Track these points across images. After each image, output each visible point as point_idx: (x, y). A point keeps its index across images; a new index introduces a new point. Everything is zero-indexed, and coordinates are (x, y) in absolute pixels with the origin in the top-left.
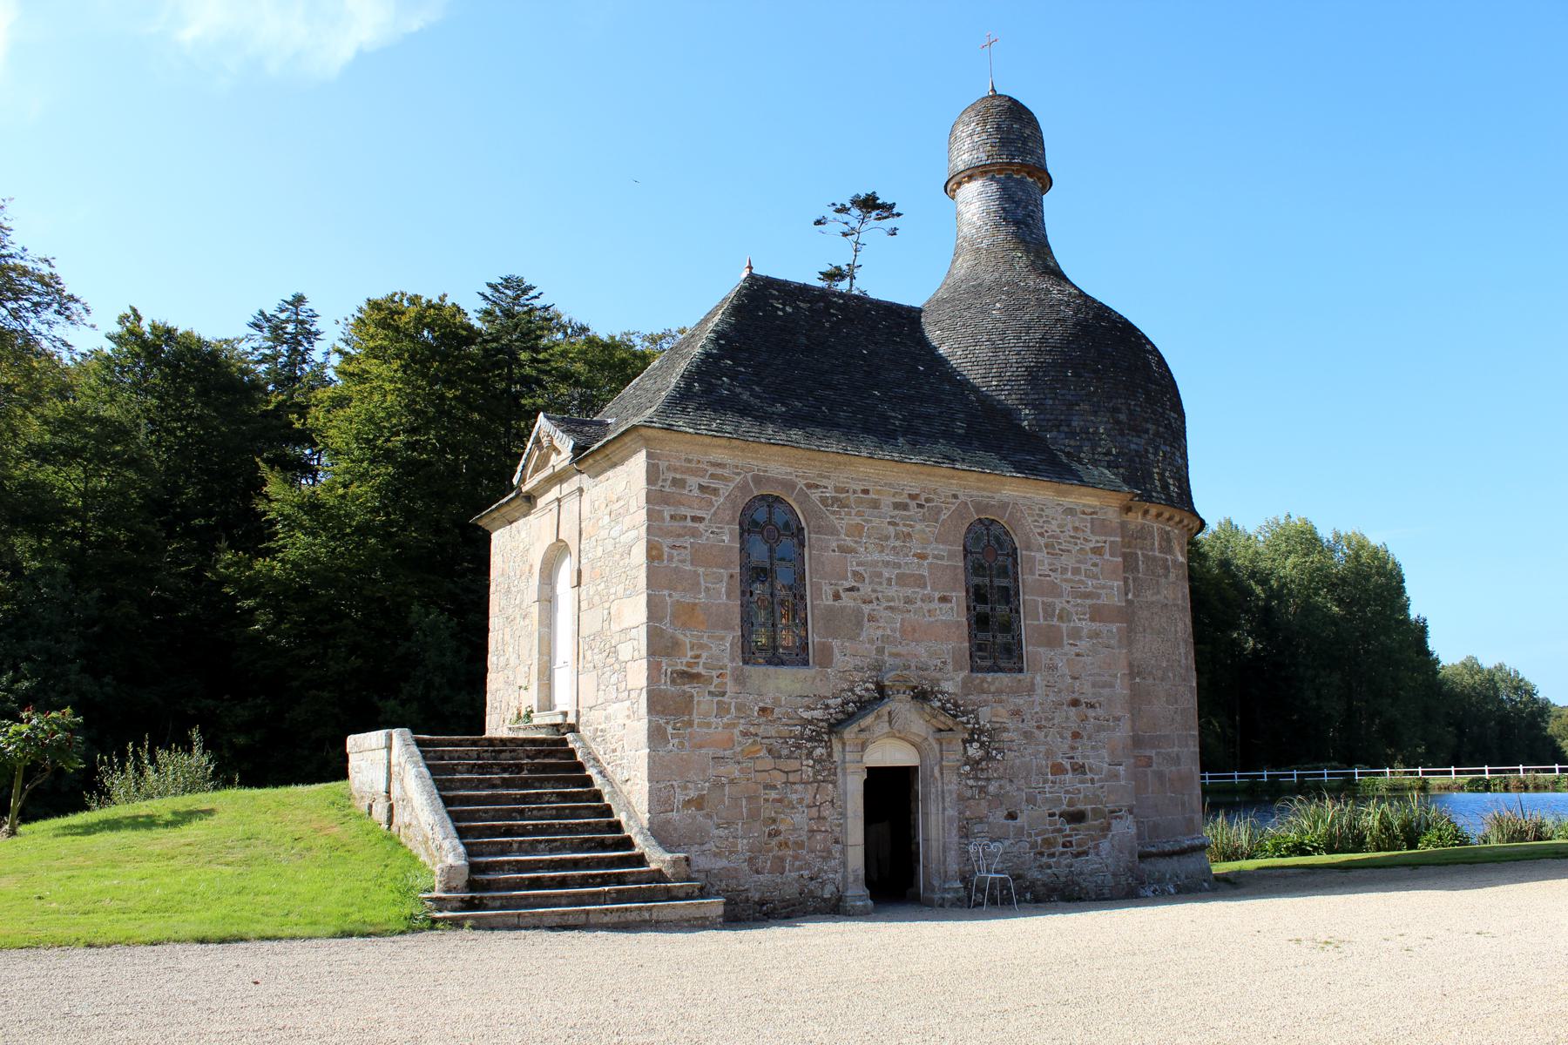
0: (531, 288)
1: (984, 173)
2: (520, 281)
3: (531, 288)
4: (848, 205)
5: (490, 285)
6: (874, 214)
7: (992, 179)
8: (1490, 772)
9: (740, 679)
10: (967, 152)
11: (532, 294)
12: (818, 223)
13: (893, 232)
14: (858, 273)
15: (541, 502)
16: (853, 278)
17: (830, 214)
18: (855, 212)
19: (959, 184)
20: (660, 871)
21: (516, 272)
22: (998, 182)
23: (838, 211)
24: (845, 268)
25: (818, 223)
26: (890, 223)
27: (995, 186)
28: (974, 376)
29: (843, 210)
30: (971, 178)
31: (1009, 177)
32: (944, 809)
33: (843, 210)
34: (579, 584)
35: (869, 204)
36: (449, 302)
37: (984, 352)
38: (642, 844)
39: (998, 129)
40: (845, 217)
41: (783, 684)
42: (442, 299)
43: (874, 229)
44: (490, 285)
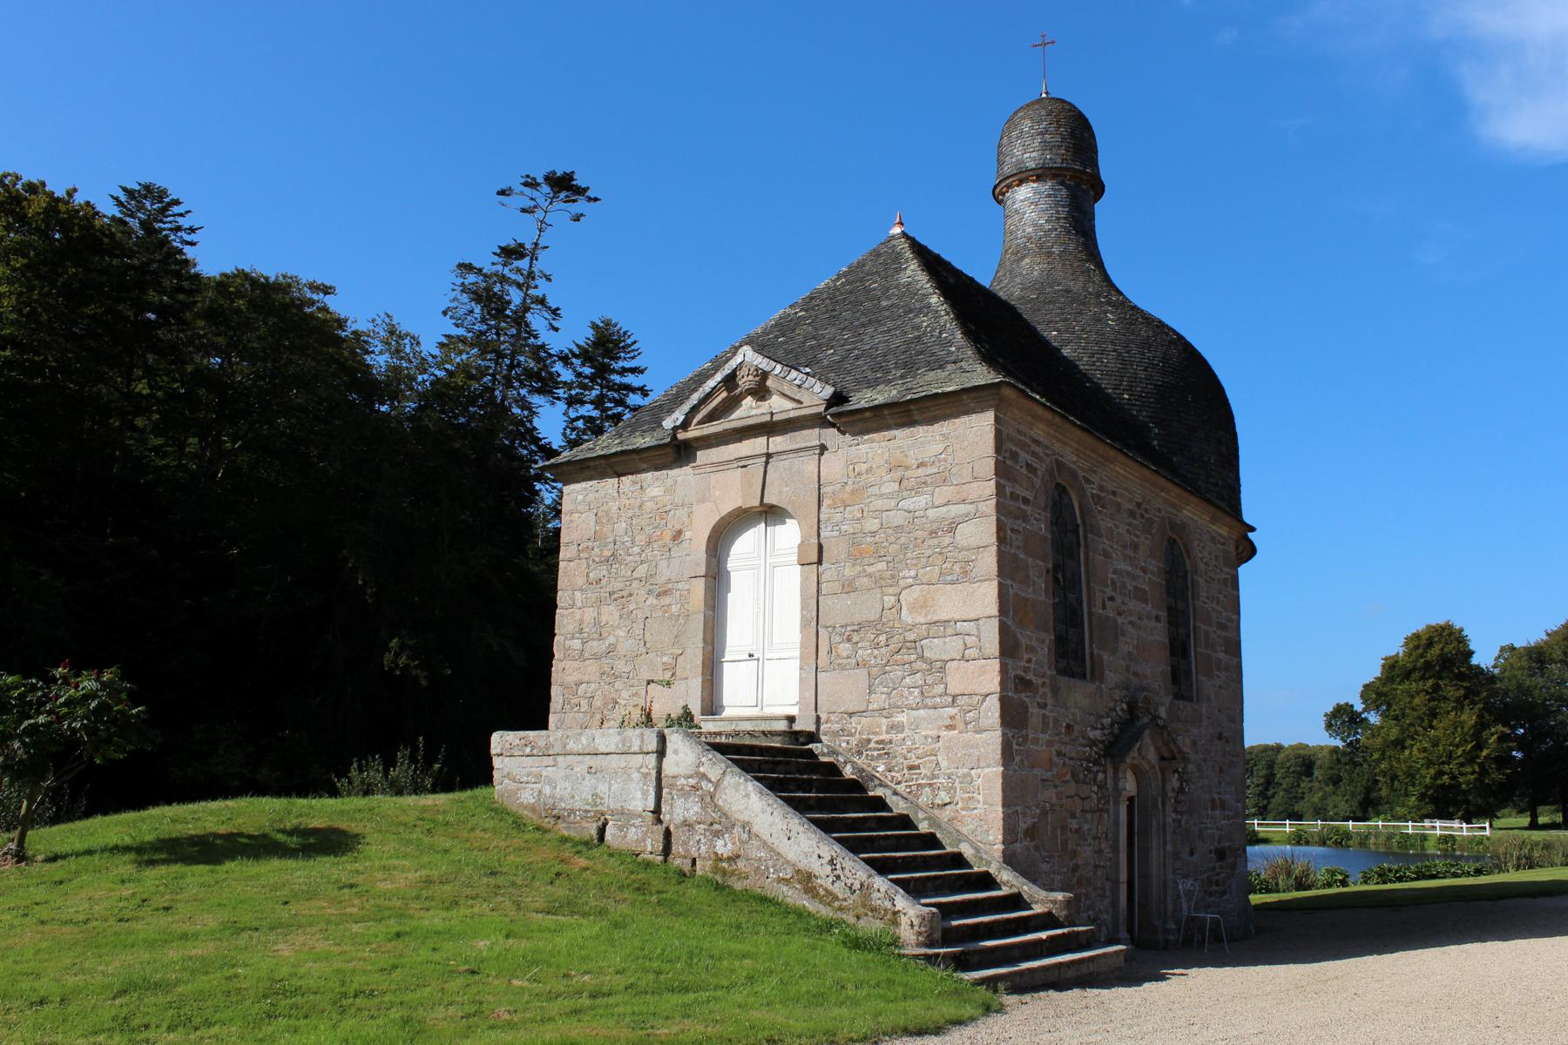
0: (177, 202)
1: (1054, 177)
2: (162, 194)
3: (177, 202)
4: (540, 180)
5: (125, 189)
6: (562, 195)
7: (1062, 183)
8: (1442, 828)
9: (1055, 691)
10: (1027, 153)
11: (176, 209)
12: (502, 193)
13: (577, 218)
14: (541, 254)
15: (702, 456)
16: (534, 258)
17: (518, 188)
18: (546, 189)
19: (1009, 187)
20: (1049, 914)
21: (159, 182)
22: (1068, 187)
23: (526, 184)
24: (528, 246)
25: (502, 193)
26: (581, 205)
27: (1064, 192)
28: (1107, 386)
29: (531, 184)
30: (1039, 178)
31: (1077, 186)
32: (1165, 844)
33: (531, 184)
34: (820, 562)
35: (563, 184)
36: (79, 199)
37: (1109, 360)
38: (1009, 881)
39: (1072, 134)
40: (535, 194)
41: (1079, 695)
42: (70, 193)
43: (560, 212)
44: (125, 189)
